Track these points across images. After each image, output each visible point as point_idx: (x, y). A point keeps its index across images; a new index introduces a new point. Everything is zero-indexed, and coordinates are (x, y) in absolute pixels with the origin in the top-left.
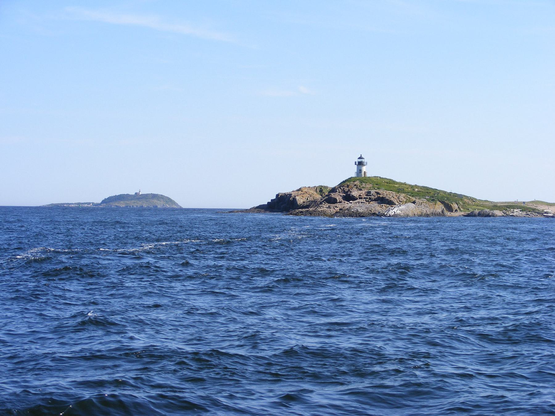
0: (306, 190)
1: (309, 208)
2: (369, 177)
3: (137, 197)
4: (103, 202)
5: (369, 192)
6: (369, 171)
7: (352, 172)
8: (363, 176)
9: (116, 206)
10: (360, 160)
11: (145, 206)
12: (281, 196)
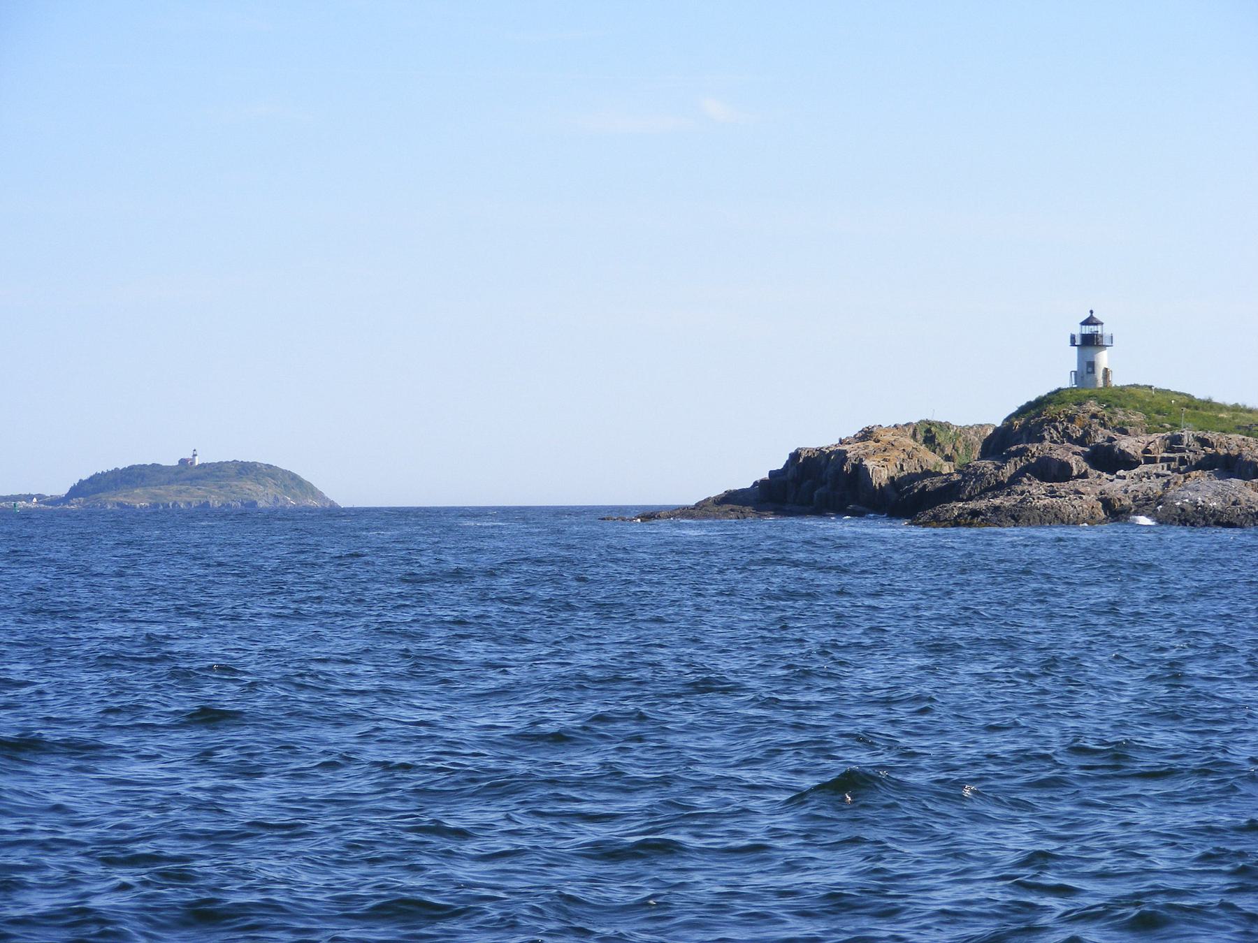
0: (889, 437)
1: (909, 500)
2: (1122, 388)
3: (187, 472)
4: (76, 491)
5: (1178, 440)
6: (1120, 366)
7: (1057, 372)
8: (1100, 383)
9: (120, 504)
10: (1088, 330)
11: (215, 502)
12: (807, 459)
